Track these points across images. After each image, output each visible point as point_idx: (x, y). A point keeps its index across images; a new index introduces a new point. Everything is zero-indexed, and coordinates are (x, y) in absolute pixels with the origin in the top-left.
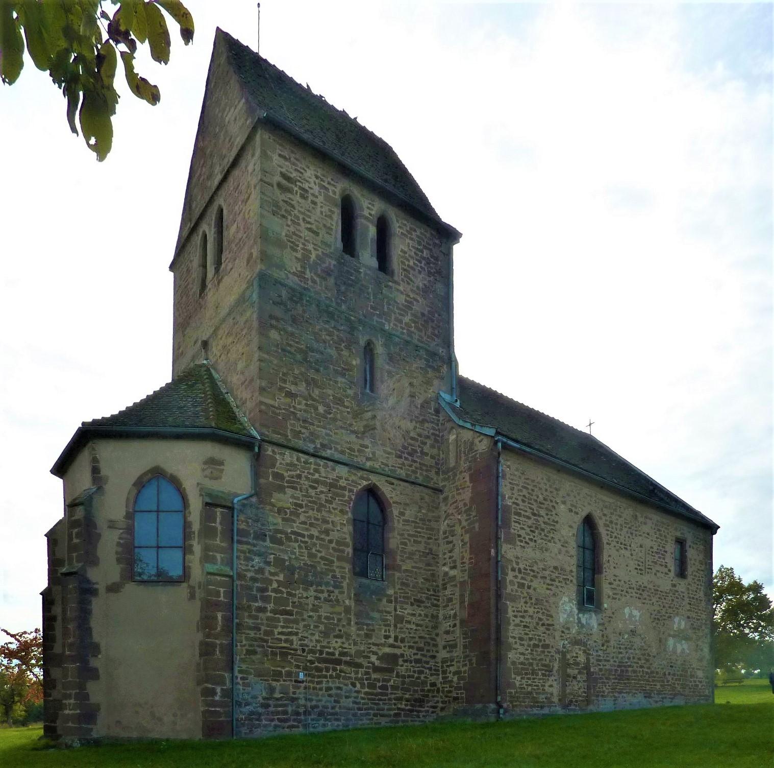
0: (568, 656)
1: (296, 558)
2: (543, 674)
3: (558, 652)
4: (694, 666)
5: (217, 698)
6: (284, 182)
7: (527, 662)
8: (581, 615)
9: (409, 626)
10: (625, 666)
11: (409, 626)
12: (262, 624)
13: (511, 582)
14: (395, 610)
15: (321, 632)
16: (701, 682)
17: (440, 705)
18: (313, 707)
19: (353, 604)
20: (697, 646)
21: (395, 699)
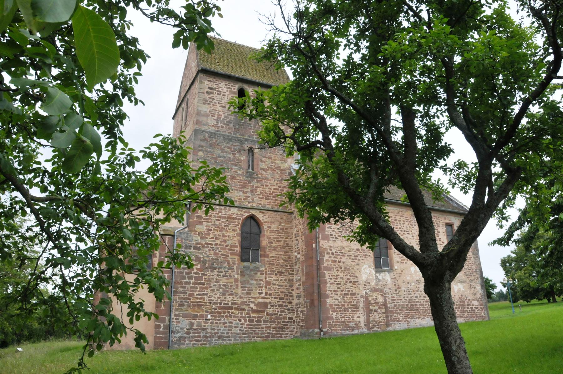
0: (370, 299)
1: (207, 256)
2: (352, 311)
3: (362, 297)
4: (470, 298)
5: (161, 330)
6: (209, 90)
7: (340, 304)
8: (378, 275)
9: (275, 287)
10: (414, 302)
11: (275, 287)
12: (188, 290)
13: (327, 261)
14: (266, 278)
15: (220, 293)
16: (477, 308)
17: (295, 330)
18: (215, 333)
19: (239, 277)
20: (471, 285)
21: (266, 327)
